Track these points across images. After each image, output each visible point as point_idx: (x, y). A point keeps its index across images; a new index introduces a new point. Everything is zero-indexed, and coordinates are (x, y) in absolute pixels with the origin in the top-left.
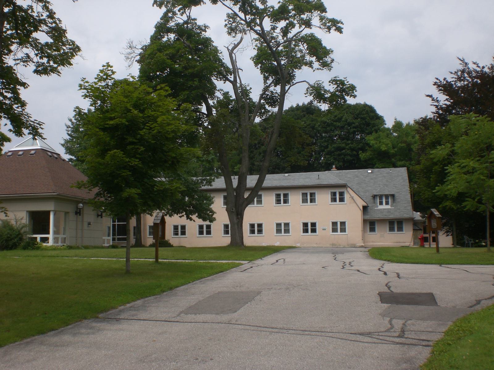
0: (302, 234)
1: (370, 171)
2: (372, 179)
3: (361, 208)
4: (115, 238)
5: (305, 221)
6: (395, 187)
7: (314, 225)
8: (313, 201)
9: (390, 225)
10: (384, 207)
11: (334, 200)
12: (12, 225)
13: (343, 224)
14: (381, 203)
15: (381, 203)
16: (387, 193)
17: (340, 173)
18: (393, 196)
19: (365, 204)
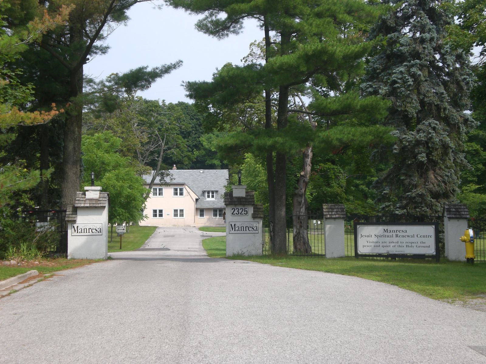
0: (173, 217)
1: (201, 172)
2: (203, 178)
3: (195, 200)
4: (311, 216)
5: (155, 209)
6: (219, 185)
7: (161, 211)
8: (161, 194)
9: (214, 212)
10: (211, 199)
11: (176, 194)
12: (304, 54)
13: (182, 211)
14: (209, 197)
15: (209, 197)
16: (213, 190)
17: (179, 171)
18: (217, 192)
19: (197, 198)
